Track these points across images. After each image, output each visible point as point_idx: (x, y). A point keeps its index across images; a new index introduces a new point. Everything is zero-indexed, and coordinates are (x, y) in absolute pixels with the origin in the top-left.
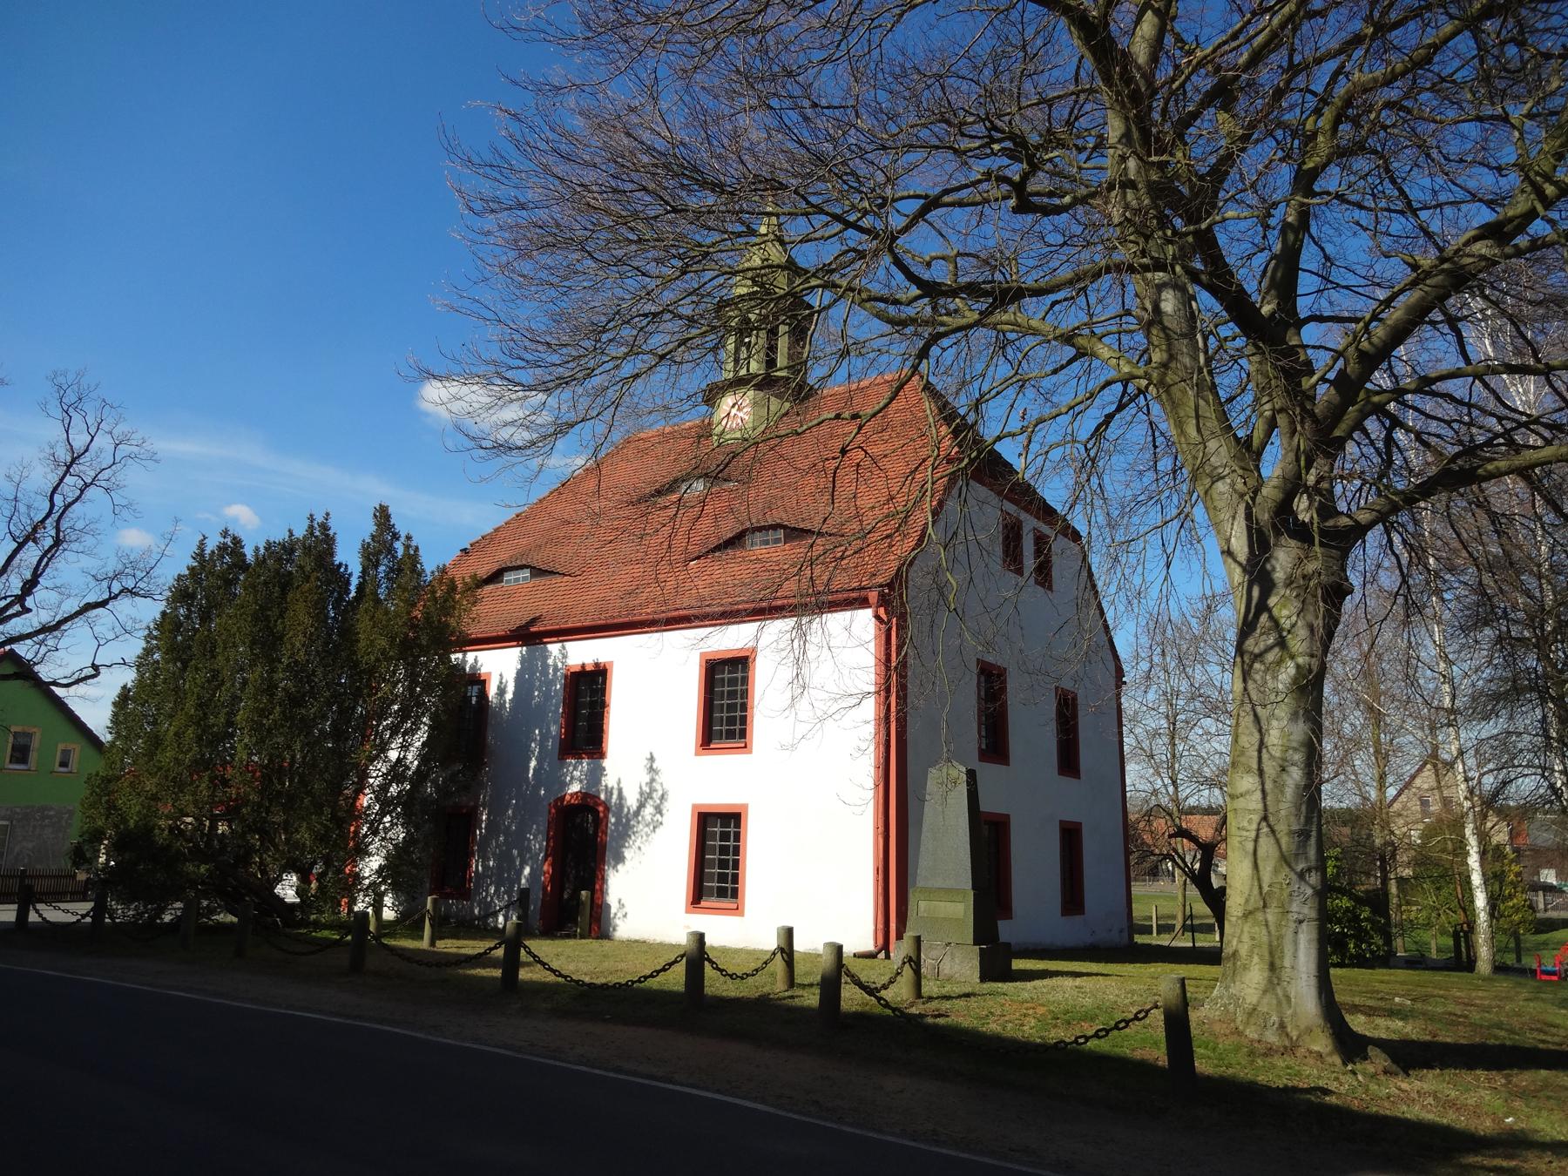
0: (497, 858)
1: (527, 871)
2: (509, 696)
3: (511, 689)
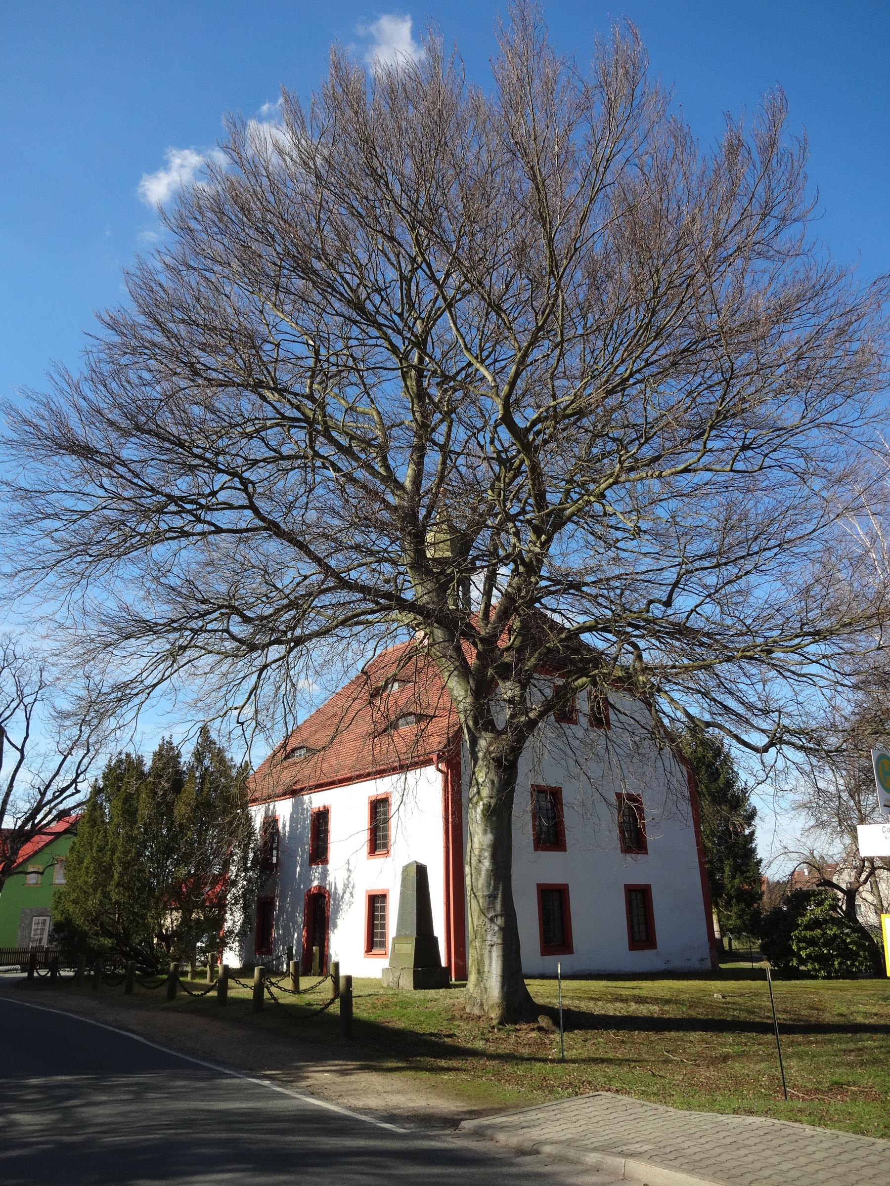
3: (288, 824)
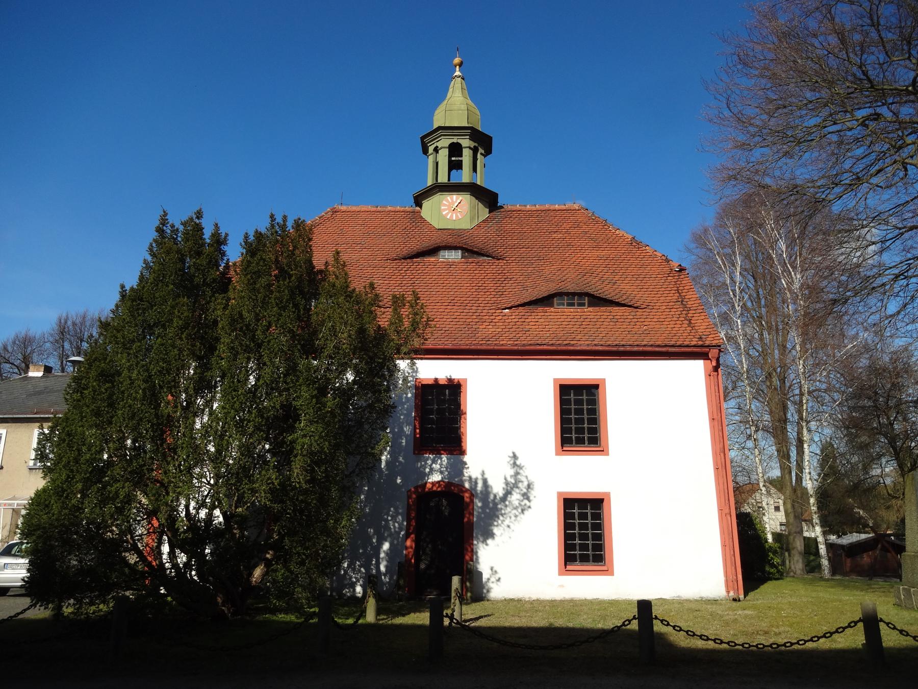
1: (386, 546)
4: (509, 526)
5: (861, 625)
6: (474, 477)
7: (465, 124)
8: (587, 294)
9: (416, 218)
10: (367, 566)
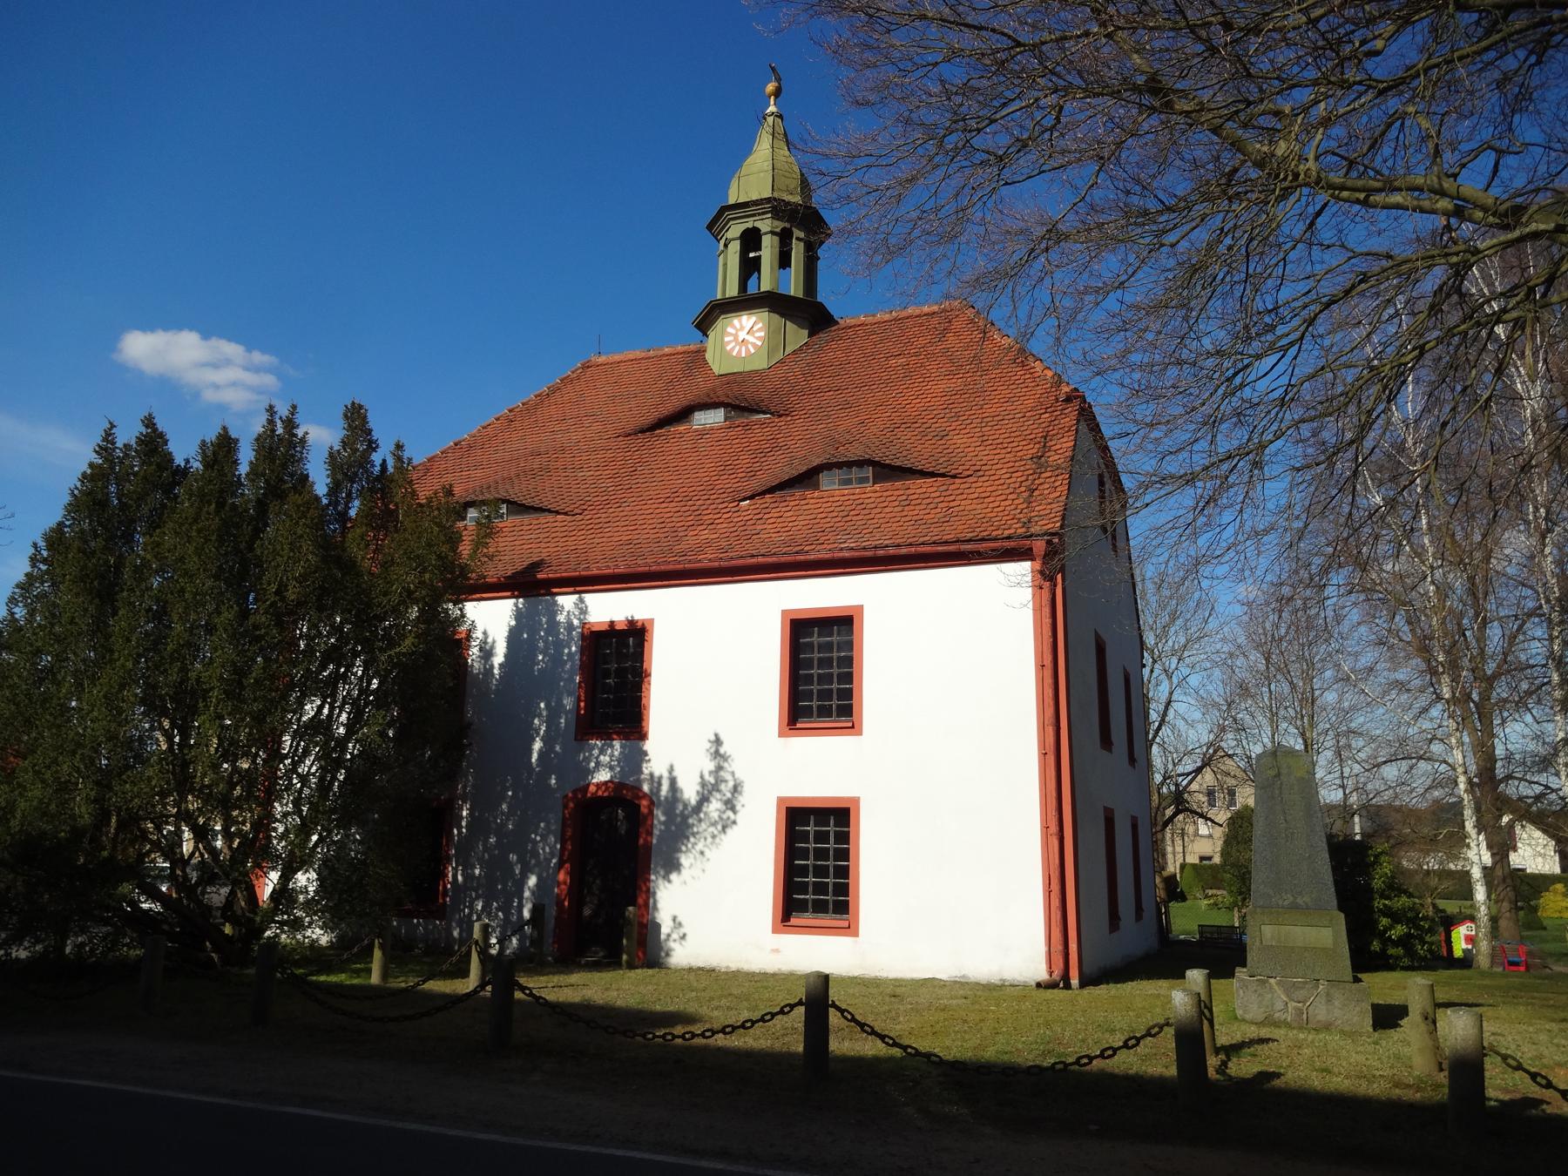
0: (488, 866)
1: (533, 881)
2: (498, 659)
4: (702, 853)
5: (802, 1009)
6: (657, 774)
7: (767, 194)
8: (870, 462)
9: (697, 358)
10: (506, 908)
